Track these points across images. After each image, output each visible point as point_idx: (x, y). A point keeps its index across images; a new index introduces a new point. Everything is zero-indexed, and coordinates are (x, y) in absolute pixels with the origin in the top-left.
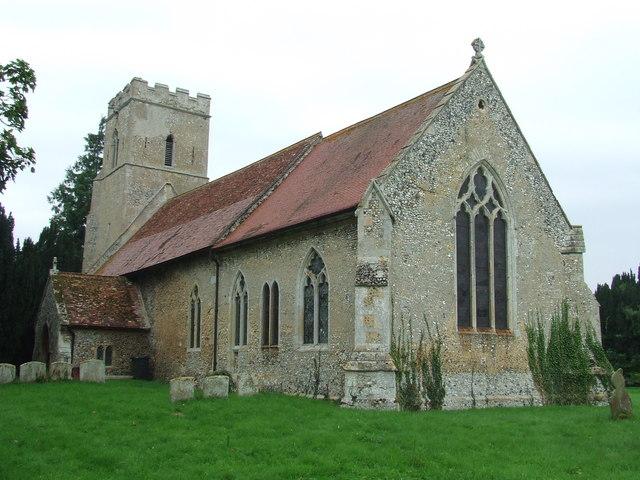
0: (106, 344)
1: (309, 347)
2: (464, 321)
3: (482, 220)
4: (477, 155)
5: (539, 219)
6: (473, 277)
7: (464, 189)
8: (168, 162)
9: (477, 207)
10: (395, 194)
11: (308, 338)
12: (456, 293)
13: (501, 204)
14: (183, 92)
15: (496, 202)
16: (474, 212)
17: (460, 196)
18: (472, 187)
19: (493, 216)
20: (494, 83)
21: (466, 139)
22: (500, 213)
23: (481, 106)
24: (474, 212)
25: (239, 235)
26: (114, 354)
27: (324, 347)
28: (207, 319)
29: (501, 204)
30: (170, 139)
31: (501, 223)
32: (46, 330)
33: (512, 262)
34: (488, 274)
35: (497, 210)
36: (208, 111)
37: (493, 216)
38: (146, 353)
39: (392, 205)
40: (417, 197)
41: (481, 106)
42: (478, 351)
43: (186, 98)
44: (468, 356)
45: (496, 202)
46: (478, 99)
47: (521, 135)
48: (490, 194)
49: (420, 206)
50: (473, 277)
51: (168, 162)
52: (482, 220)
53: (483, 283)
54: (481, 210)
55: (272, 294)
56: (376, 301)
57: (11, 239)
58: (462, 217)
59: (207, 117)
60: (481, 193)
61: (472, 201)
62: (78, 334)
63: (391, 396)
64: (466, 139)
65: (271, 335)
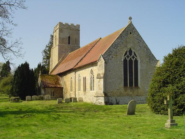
0: (53, 91)
1: (91, 91)
2: (125, 85)
3: (131, 61)
4: (129, 46)
5: (147, 60)
6: (128, 74)
7: (126, 54)
8: (69, 43)
9: (129, 58)
10: (107, 57)
11: (91, 90)
12: (123, 78)
13: (136, 57)
14: (72, 25)
15: (135, 56)
16: (128, 60)
17: (125, 56)
18: (128, 53)
19: (133, 60)
20: (134, 27)
21: (126, 42)
22: (136, 59)
23: (131, 33)
24: (128, 60)
25: (77, 66)
26: (55, 94)
27: (93, 91)
28: (73, 85)
29: (136, 57)
30: (69, 37)
31: (136, 61)
32: (159, 74)
33: (139, 70)
34: (133, 73)
35: (135, 58)
36: (79, 29)
37: (133, 60)
38: (106, 97)
39: (106, 59)
40: (113, 57)
41: (131, 33)
42: (129, 92)
43: (73, 26)
44: (126, 93)
45: (135, 56)
46: (130, 32)
47: (142, 39)
48: (133, 54)
49: (113, 59)
50: (128, 74)
51: (69, 43)
52: (131, 61)
53: (131, 76)
54: (131, 59)
55: (85, 79)
56: (101, 81)
57: (29, 68)
58: (125, 61)
59: (79, 30)
60: (131, 54)
61: (128, 57)
62: (46, 89)
63: (103, 102)
64: (126, 42)
65: (85, 89)
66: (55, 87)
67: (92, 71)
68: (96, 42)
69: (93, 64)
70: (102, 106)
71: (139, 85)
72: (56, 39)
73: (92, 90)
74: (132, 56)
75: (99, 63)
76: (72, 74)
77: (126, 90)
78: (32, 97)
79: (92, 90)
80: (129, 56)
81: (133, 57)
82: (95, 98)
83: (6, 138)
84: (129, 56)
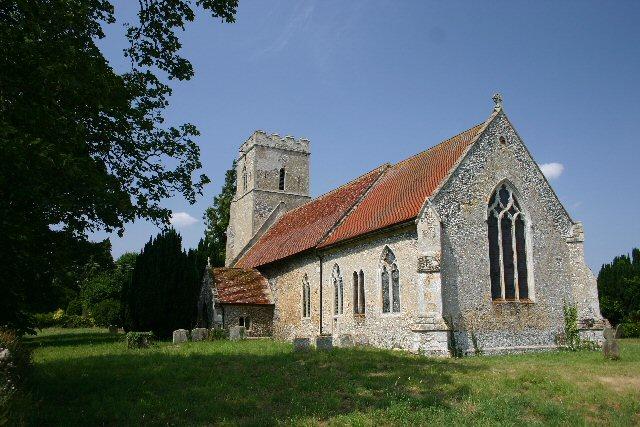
1: (386, 315)
3: (506, 222)
17: (490, 205)
18: (498, 199)
22: (519, 216)
24: (500, 216)
30: (282, 171)
31: (520, 223)
52: (506, 222)
54: (506, 214)
55: (359, 277)
57: (180, 246)
58: (492, 221)
61: (499, 209)
66: (252, 304)
67: (389, 256)
68: (375, 177)
69: (394, 230)
70: (445, 362)
71: (532, 296)
72: (245, 177)
73: (391, 309)
74: (509, 206)
75: (421, 226)
76: (312, 268)
77: (498, 312)
78: (190, 332)
79: (391, 309)
80: (501, 205)
81: (512, 211)
82: (417, 337)
83: (529, 425)
84: (501, 205)
